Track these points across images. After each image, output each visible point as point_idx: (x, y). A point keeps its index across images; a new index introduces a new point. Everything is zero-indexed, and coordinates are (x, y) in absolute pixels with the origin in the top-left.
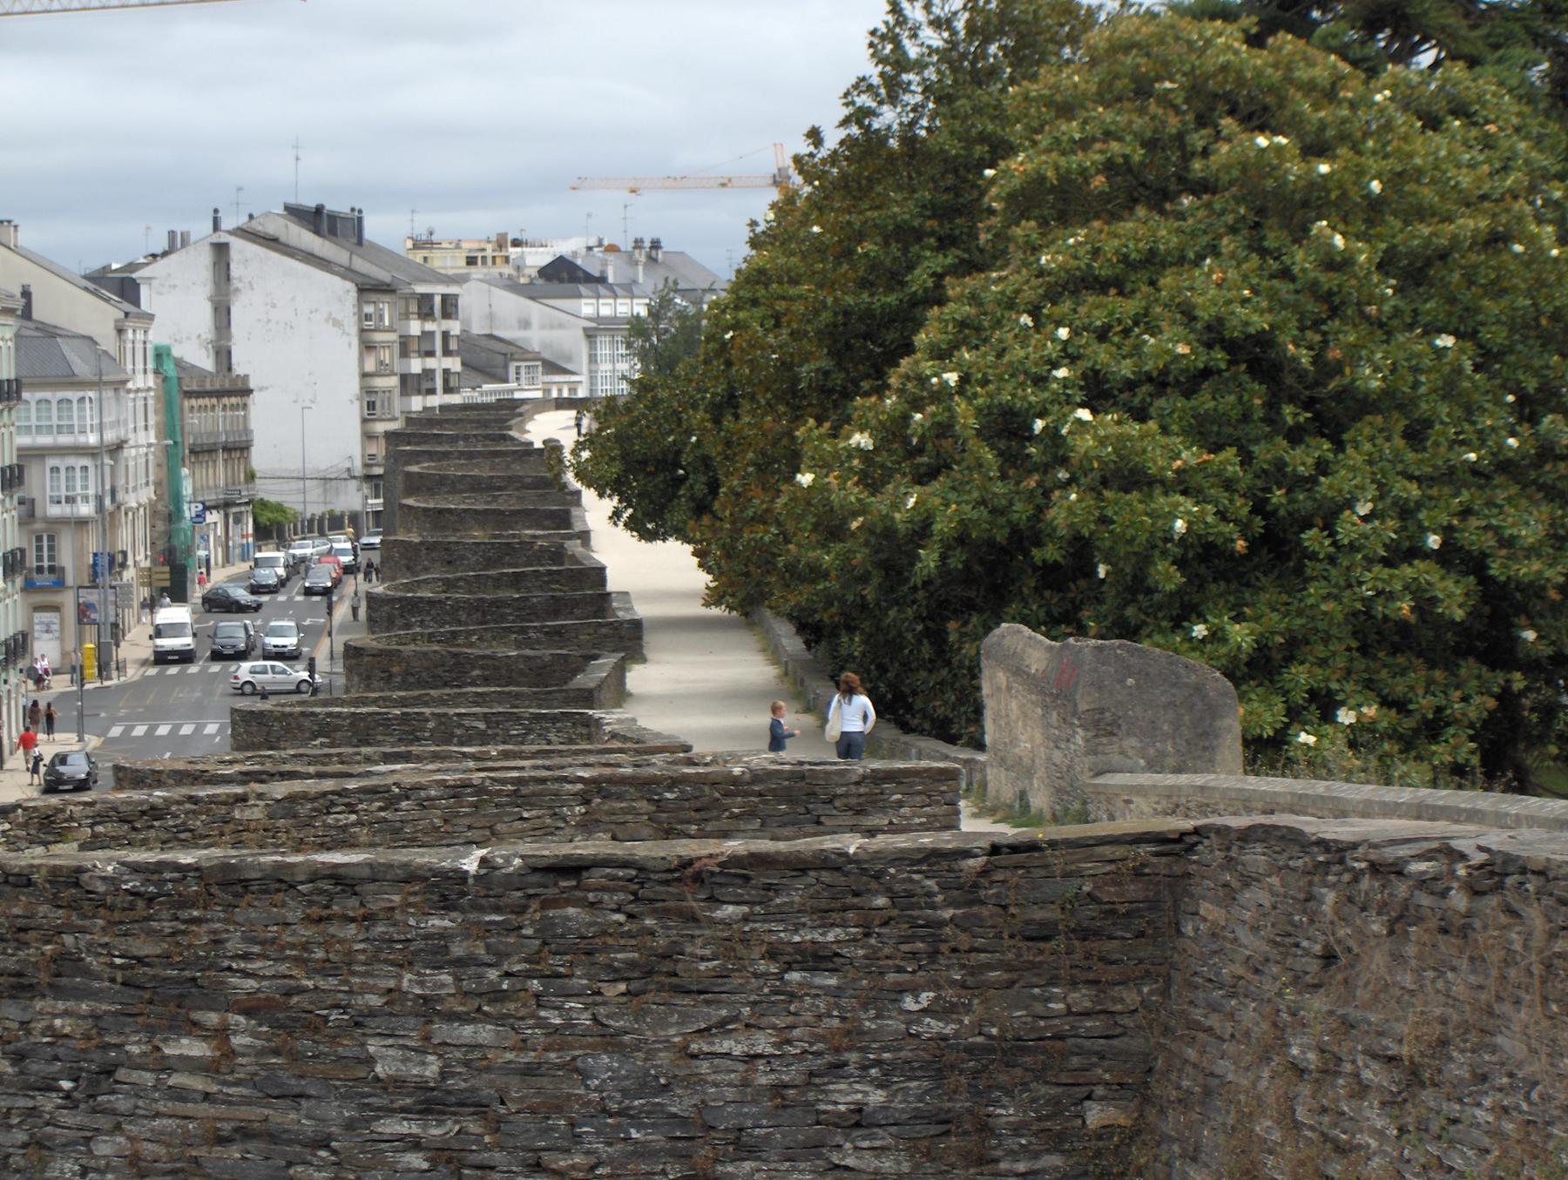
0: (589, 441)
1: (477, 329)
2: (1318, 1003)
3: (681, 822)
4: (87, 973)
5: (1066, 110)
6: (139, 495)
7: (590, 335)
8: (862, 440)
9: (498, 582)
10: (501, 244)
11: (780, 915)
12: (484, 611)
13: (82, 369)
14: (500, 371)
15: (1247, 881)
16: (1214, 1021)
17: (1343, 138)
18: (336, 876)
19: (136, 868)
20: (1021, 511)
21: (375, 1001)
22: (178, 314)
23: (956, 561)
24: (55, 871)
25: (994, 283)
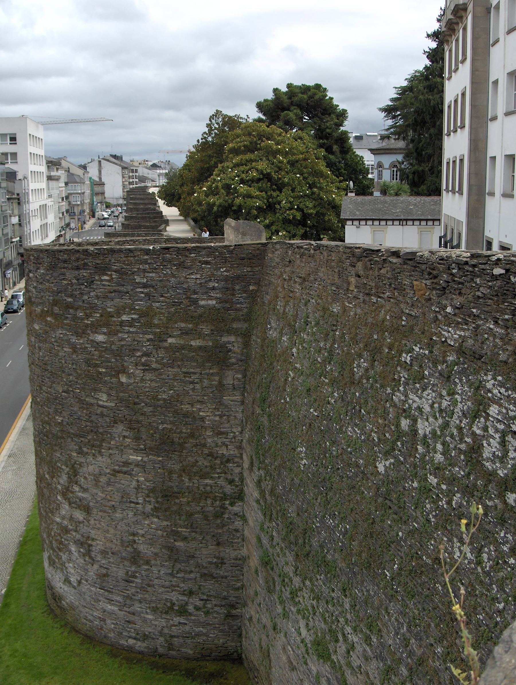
0: (159, 192)
1: (141, 175)
2: (288, 269)
4: (89, 266)
5: (238, 137)
6: (87, 201)
7: (159, 176)
8: (205, 189)
9: (145, 214)
10: (144, 161)
11: (200, 256)
12: (143, 218)
13: (78, 180)
15: (276, 250)
16: (271, 272)
17: (282, 142)
18: (130, 250)
19: (97, 249)
20: (230, 201)
21: (136, 270)
22: (93, 172)
23: (220, 209)
24: (83, 250)
25: (226, 164)
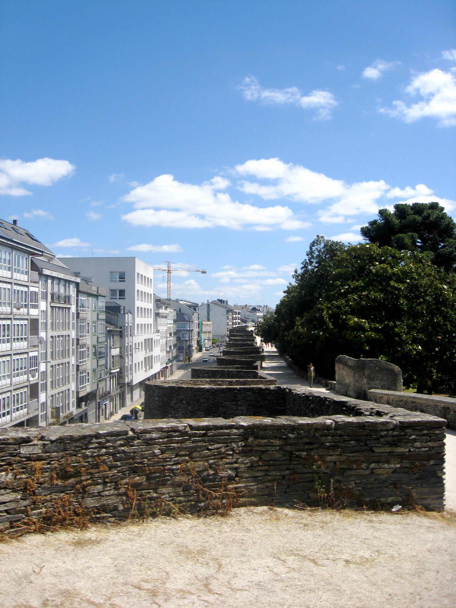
3: (297, 451)
13: (187, 319)
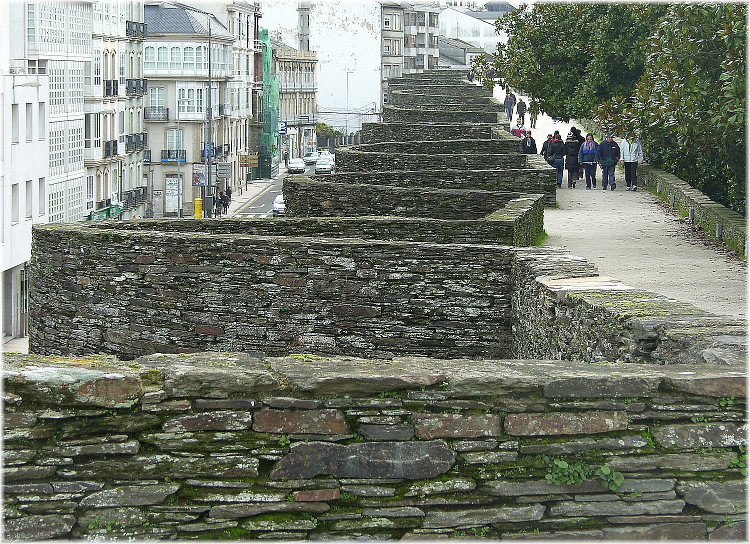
1: (449, 35)
14: (461, 59)
